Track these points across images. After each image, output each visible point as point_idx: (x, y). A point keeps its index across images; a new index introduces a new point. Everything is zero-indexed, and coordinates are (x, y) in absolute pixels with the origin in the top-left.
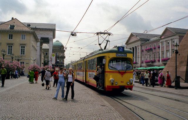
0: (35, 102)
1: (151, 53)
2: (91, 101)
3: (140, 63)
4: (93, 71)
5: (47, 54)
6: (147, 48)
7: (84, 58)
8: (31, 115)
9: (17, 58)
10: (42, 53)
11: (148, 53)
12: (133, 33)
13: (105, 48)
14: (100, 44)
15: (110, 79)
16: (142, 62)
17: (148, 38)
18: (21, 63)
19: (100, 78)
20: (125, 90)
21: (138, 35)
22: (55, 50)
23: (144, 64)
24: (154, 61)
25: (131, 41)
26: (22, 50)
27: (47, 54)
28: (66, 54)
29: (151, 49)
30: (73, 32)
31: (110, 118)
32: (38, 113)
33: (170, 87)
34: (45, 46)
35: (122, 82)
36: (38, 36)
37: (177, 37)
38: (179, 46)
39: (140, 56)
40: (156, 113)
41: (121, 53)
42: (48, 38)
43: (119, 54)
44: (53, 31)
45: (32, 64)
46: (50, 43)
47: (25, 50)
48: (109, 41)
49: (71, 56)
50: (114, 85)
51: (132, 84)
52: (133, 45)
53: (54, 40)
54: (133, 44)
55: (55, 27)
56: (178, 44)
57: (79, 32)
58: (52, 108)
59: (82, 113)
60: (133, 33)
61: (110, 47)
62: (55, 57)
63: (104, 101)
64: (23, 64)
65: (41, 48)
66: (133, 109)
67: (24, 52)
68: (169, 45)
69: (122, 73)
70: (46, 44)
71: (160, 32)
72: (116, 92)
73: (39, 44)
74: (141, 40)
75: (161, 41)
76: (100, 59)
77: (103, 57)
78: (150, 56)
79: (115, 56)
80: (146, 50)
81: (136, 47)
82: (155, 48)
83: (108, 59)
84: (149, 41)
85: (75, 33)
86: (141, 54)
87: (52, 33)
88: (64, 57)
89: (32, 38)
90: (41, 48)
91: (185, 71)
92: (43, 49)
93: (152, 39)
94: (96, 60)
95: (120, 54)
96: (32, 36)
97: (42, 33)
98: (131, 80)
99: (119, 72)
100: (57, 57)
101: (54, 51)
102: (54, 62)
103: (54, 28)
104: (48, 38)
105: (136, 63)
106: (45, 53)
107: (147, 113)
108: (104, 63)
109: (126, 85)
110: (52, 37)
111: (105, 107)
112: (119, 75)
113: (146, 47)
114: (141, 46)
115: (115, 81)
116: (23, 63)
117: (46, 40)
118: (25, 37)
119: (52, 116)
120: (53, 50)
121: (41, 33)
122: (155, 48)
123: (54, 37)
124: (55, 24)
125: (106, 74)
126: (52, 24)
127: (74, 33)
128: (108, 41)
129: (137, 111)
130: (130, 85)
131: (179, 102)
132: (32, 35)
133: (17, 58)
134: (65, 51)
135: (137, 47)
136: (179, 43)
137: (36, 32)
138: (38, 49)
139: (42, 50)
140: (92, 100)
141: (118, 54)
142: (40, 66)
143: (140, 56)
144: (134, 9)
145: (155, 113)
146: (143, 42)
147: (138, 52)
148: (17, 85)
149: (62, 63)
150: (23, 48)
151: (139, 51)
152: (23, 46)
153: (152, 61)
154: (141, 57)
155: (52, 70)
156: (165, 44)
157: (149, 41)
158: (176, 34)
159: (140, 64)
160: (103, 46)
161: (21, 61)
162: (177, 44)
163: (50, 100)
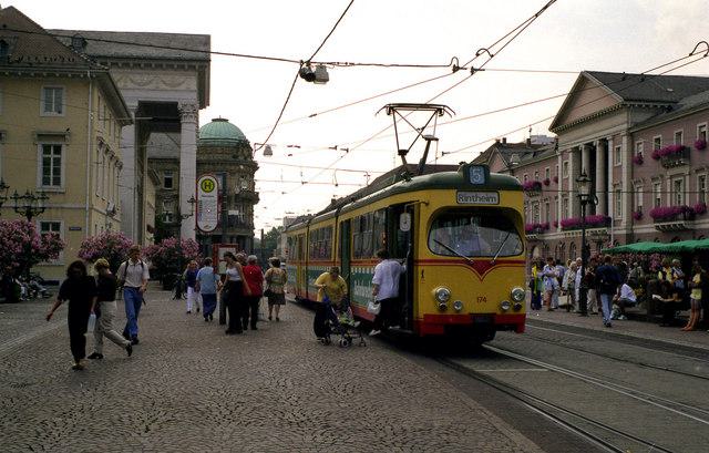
0: (120, 440)
1: (686, 170)
2: (434, 433)
3: (625, 220)
5: (168, 182)
6: (663, 146)
9: (21, 203)
11: (670, 172)
12: (589, 76)
14: (403, 153)
15: (433, 291)
16: (637, 217)
18: (45, 226)
20: (498, 333)
21: (607, 79)
22: (209, 162)
23: (648, 228)
24: (547, 227)
25: (579, 113)
26: (46, 162)
28: (263, 180)
29: (682, 152)
30: (308, 63)
33: (671, 325)
34: (159, 142)
36: (123, 93)
39: (625, 185)
45: (97, 227)
46: (184, 126)
47: (63, 161)
48: (437, 140)
49: (285, 196)
50: (450, 312)
51: (518, 308)
52: (592, 134)
53: (205, 117)
54: (589, 129)
60: (591, 73)
62: (215, 193)
63: (506, 432)
64: (55, 233)
65: (141, 153)
67: (57, 172)
68: (621, 166)
69: (482, 266)
70: (163, 136)
72: (458, 341)
73: (129, 132)
77: (410, 208)
78: (678, 183)
80: (657, 157)
81: (604, 142)
82: (547, 183)
83: (425, 216)
84: (670, 109)
85: (321, 67)
86: (632, 175)
87: (193, 83)
88: (254, 198)
89: (96, 103)
92: (151, 160)
93: (690, 102)
96: (97, 94)
98: (515, 293)
100: (224, 199)
101: (202, 167)
102: (210, 222)
105: (607, 221)
106: (162, 177)
110: (193, 97)
112: (469, 275)
113: (679, 134)
114: (631, 136)
116: (56, 226)
118: (59, 98)
120: (199, 163)
121: (138, 78)
122: (547, 183)
123: (204, 101)
124: (208, 38)
125: (420, 269)
127: (314, 70)
128: (429, 139)
130: (512, 312)
132: (96, 90)
133: (21, 203)
134: (255, 167)
135: (610, 143)
137: (116, 75)
138: (128, 156)
139: (146, 161)
142: (140, 242)
143: (625, 185)
146: (641, 117)
147: (614, 168)
148: (21, 340)
150: (52, 156)
151: (620, 159)
152: (52, 144)
153: (691, 210)
154: (632, 193)
155: (234, 277)
159: (623, 224)
161: (45, 217)
163: (207, 431)
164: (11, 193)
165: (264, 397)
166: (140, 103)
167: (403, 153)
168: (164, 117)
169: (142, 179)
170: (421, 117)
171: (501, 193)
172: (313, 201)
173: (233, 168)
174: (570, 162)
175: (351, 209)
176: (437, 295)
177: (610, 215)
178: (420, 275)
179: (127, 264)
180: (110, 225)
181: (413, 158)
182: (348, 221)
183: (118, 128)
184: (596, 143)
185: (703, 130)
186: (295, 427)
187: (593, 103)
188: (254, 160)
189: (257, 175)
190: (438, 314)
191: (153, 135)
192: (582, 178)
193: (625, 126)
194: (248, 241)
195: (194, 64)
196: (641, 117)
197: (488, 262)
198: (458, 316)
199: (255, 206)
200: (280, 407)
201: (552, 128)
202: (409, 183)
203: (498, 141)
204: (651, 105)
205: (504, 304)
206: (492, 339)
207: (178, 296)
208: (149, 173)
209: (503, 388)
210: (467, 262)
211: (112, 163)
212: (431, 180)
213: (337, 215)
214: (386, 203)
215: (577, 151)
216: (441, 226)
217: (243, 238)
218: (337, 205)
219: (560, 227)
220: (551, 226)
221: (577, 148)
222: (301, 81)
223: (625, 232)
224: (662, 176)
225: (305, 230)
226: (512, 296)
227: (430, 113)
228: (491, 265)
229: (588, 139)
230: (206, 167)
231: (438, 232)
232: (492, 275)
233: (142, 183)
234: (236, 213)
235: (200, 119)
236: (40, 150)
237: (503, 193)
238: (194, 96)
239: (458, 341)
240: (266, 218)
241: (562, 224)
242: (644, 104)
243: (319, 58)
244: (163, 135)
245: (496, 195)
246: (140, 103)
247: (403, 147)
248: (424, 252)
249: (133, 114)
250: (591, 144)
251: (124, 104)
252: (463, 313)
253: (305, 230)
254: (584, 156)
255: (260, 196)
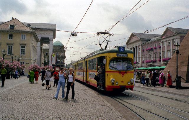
0: (35, 102)
1: (152, 53)
2: (91, 101)
3: (140, 63)
4: (94, 71)
5: (47, 54)
6: (148, 48)
7: (85, 58)
8: (31, 115)
9: (17, 58)
10: (42, 53)
11: (149, 53)
12: (133, 33)
13: (106, 48)
14: (100, 44)
15: (111, 79)
16: (143, 62)
17: (149, 38)
18: (21, 63)
19: (101, 78)
20: (125, 90)
21: (138, 35)
22: (55, 50)
23: (145, 64)
24: (155, 61)
25: (132, 41)
26: (22, 50)
27: (47, 54)
28: (66, 54)
29: (152, 49)
30: (73, 32)
31: (111, 118)
32: (39, 113)
33: (170, 87)
34: (45, 46)
35: (122, 82)
36: (38, 36)
37: (178, 37)
38: (179, 46)
39: (140, 56)
40: (157, 113)
41: (121, 53)
42: (49, 38)
43: (120, 54)
44: (54, 31)
45: (32, 64)
46: (50, 43)
47: (25, 50)
48: (110, 41)
49: (72, 56)
50: (115, 85)
51: (132, 84)
52: (134, 45)
53: (55, 40)
54: (134, 44)
55: (55, 27)
56: (179, 44)
57: (80, 32)
58: (52, 108)
59: (83, 113)
60: (134, 33)
61: (111, 47)
62: (55, 57)
63: (104, 101)
64: (23, 64)
65: (41, 48)
66: (134, 109)
67: (24, 52)
68: (170, 45)
69: (123, 73)
70: (46, 44)
71: (161, 32)
72: (116, 92)
73: (39, 44)
74: (142, 40)
75: (162, 41)
76: (101, 59)
77: (104, 57)
78: (151, 56)
79: (116, 56)
80: (147, 50)
81: (137, 47)
82: (156, 48)
83: (108, 59)
84: (149, 41)
85: (75, 33)
86: (142, 54)
87: (52, 33)
88: (65, 57)
89: (32, 38)
90: (41, 48)
91: (186, 71)
92: (43, 49)
93: (153, 39)
94: (96, 60)
95: (121, 54)
96: (32, 36)
97: (42, 33)
98: (132, 80)
99: (120, 72)
100: (57, 57)
101: (54, 51)
102: (54, 62)
103: (54, 28)
104: (49, 38)
105: (137, 63)
106: (45, 53)
107: (148, 113)
108: (104, 63)
109: (127, 85)
110: (52, 37)
111: (106, 107)
112: (119, 75)
113: (147, 47)
114: (142, 46)
115: (116, 81)
116: (24, 63)
117: (46, 40)
118: (25, 37)
119: (52, 116)
120: (53, 50)
121: (41, 33)
122: (156, 48)
123: (54, 37)
124: (56, 24)
125: (107, 74)
126: (52, 24)
127: (74, 33)
128: (108, 41)
129: (137, 111)
130: (130, 85)
131: (179, 102)
132: (32, 35)
133: (17, 58)
134: (65, 51)
135: (138, 47)
136: (180, 43)
137: (36, 32)
138: (38, 49)
139: (42, 50)
140: (92, 100)
141: (119, 54)
142: (41, 66)
143: (140, 56)
144: (135, 9)
145: (155, 113)
146: (144, 42)
147: (139, 52)
148: (17, 85)
149: (62, 63)
150: (23, 48)
151: (140, 51)
152: (23, 46)
153: (153, 61)
154: (142, 57)
155: (52, 70)
156: (166, 44)
157: (149, 41)
158: (177, 34)
159: (140, 64)
160: (103, 46)
161: (21, 61)
162: (178, 44)
163: (51, 100)
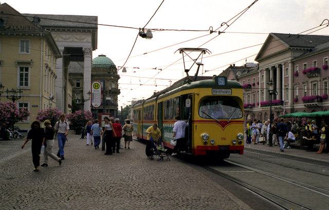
0: (56, 204)
1: (318, 79)
2: (201, 201)
3: (290, 102)
5: (78, 85)
6: (308, 68)
9: (10, 94)
11: (311, 80)
12: (273, 35)
14: (187, 71)
15: (201, 135)
16: (296, 100)
18: (21, 105)
20: (231, 154)
21: (281, 36)
22: (97, 75)
23: (301, 105)
24: (254, 105)
25: (269, 53)
26: (21, 75)
28: (122, 84)
29: (317, 70)
30: (143, 29)
33: (311, 151)
34: (74, 66)
36: (57, 43)
39: (290, 86)
45: (45, 105)
46: (85, 58)
47: (29, 75)
48: (203, 65)
49: (132, 91)
50: (209, 145)
51: (240, 143)
52: (275, 62)
53: (95, 54)
54: (273, 60)
60: (274, 34)
62: (100, 90)
63: (235, 200)
64: (25, 108)
65: (65, 71)
67: (26, 80)
68: (288, 77)
69: (224, 124)
70: (76, 63)
72: (212, 158)
73: (60, 61)
77: (190, 96)
78: (315, 85)
80: (305, 73)
81: (280, 66)
82: (254, 85)
83: (197, 100)
84: (311, 51)
85: (149, 31)
86: (293, 81)
87: (89, 39)
88: (118, 92)
89: (45, 48)
92: (70, 74)
93: (320, 47)
96: (45, 43)
98: (239, 136)
100: (104, 92)
101: (94, 77)
102: (97, 103)
105: (281, 103)
106: (75, 82)
110: (90, 45)
112: (218, 127)
113: (315, 62)
114: (293, 63)
116: (26, 105)
118: (27, 46)
120: (92, 76)
121: (64, 36)
122: (254, 85)
123: (94, 47)
124: (96, 17)
125: (195, 125)
127: (146, 32)
128: (199, 65)
130: (237, 145)
132: (44, 42)
133: (10, 94)
134: (118, 77)
135: (283, 66)
137: (54, 35)
138: (59, 72)
139: (68, 75)
142: (65, 112)
143: (290, 86)
146: (297, 54)
147: (285, 78)
148: (10, 157)
150: (24, 72)
151: (288, 74)
152: (24, 67)
153: (321, 97)
154: (293, 89)
155: (109, 128)
159: (289, 104)
161: (21, 101)
164: (5, 89)
165: (122, 184)
166: (65, 48)
167: (187, 71)
168: (76, 54)
169: (66, 83)
170: (195, 54)
171: (233, 89)
172: (145, 93)
173: (108, 78)
174: (265, 75)
175: (163, 97)
176: (203, 137)
177: (283, 99)
178: (195, 128)
179: (59, 122)
180: (51, 104)
181: (192, 73)
182: (162, 103)
183: (55, 59)
184: (277, 66)
185: (326, 60)
186: (137, 198)
187: (275, 48)
188: (118, 74)
189: (119, 81)
190: (203, 145)
191: (71, 63)
192: (270, 83)
193: (290, 58)
194: (115, 112)
195: (90, 30)
196: (297, 54)
197: (226, 121)
198: (213, 146)
199: (118, 96)
200: (130, 189)
201: (256, 59)
202: (190, 85)
203: (231, 66)
204: (302, 48)
205: (234, 141)
206: (228, 157)
207: (83, 137)
208: (69, 80)
209: (233, 180)
210: (217, 121)
211: (52, 76)
212: (200, 83)
213: (156, 100)
214: (179, 94)
215: (268, 70)
216: (205, 105)
217: (113, 110)
218: (156, 95)
219: (260, 105)
220: (256, 105)
221: (268, 68)
222: (140, 38)
223: (290, 108)
224: (307, 82)
225: (142, 107)
226: (237, 137)
227: (200, 52)
228: (228, 123)
229: (273, 65)
230: (96, 77)
231: (203, 108)
232: (229, 128)
233: (66, 85)
234: (109, 99)
235: (93, 55)
236: (19, 69)
237: (233, 90)
238: (90, 44)
239: (212, 158)
240: (124, 101)
241: (261, 104)
242: (299, 48)
243: (148, 27)
244: (76, 63)
245: (230, 90)
246: (65, 48)
247: (187, 68)
248: (197, 117)
249: (62, 53)
250: (274, 67)
251: (57, 48)
252: (215, 145)
253: (142, 107)
254: (271, 72)
255: (121, 91)
